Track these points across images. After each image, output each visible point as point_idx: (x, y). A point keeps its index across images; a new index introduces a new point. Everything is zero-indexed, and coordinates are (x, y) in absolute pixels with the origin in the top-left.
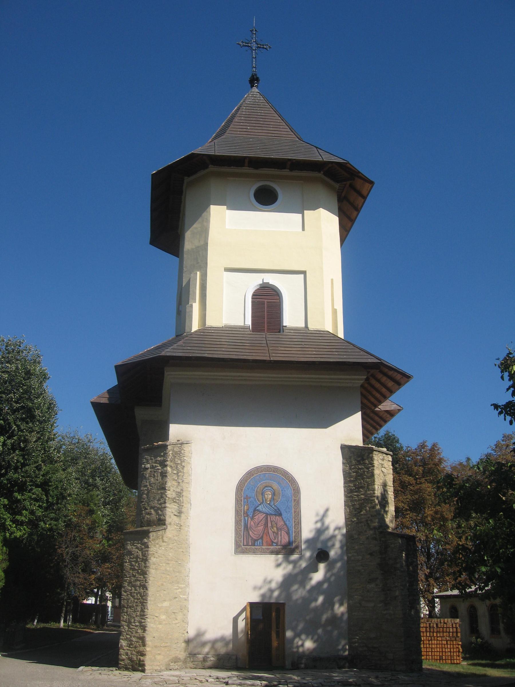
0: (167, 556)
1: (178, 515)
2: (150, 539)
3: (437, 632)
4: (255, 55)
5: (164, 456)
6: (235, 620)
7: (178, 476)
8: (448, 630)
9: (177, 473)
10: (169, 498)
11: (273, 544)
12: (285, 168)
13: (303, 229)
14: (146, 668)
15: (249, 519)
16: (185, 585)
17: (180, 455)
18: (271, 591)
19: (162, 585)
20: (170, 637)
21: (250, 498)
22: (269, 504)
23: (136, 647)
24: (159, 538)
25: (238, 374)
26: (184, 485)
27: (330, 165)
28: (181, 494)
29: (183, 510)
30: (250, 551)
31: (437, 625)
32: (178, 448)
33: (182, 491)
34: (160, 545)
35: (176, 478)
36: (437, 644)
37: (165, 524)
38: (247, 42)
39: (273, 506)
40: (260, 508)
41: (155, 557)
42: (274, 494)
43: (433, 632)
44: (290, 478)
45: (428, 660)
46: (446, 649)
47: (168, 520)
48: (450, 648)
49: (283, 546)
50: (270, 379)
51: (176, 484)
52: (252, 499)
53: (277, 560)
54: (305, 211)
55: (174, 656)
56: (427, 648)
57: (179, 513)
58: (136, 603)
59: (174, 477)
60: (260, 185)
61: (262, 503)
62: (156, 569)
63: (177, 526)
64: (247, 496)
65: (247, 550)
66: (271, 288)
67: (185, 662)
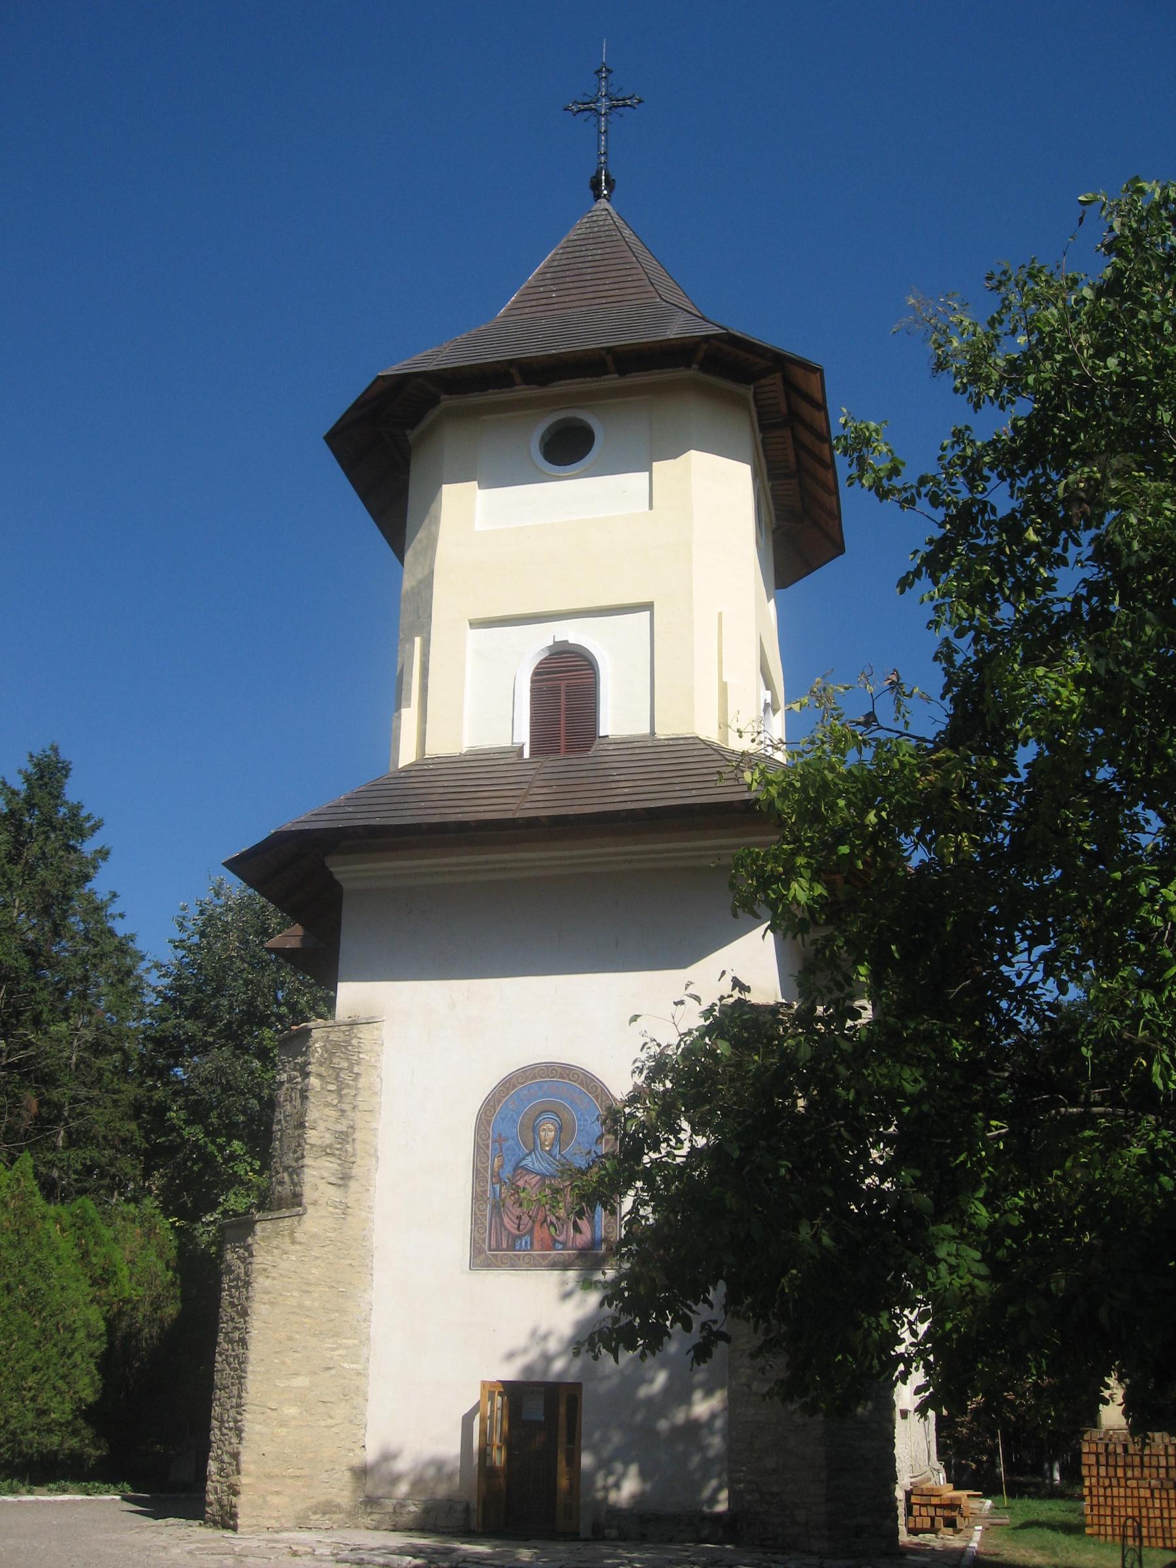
0: (305, 1276)
1: (340, 1182)
2: (256, 1237)
3: (1125, 1466)
4: (606, 126)
5: (304, 1054)
6: (467, 1421)
7: (341, 1097)
8: (1154, 1463)
10: (312, 1146)
11: (557, 1245)
13: (651, 507)
14: (239, 1521)
16: (356, 1342)
17: (348, 1050)
18: (548, 1359)
19: (290, 1339)
20: (311, 1455)
21: (507, 1139)
22: (549, 1152)
23: (227, 1476)
25: (483, 858)
26: (358, 1118)
27: (705, 346)
28: (347, 1136)
29: (354, 1172)
30: (503, 1263)
31: (1125, 1448)
32: (341, 1034)
33: (350, 1130)
35: (335, 1102)
36: (1126, 1497)
37: (300, 1205)
38: (587, 100)
40: (528, 1162)
41: (268, 1277)
42: (560, 1129)
43: (1116, 1466)
44: (599, 1090)
45: (1102, 1538)
46: (1151, 1511)
47: (308, 1194)
48: (1161, 1510)
49: (580, 1249)
50: (603, 859)
51: (334, 1114)
52: (510, 1142)
53: (564, 1283)
54: (654, 464)
55: (322, 1499)
56: (1099, 1505)
58: (233, 1378)
59: (329, 1099)
60: (560, 418)
61: (534, 1150)
62: (272, 1304)
63: (336, 1208)
65: (496, 1258)
66: (576, 653)
67: (352, 1514)
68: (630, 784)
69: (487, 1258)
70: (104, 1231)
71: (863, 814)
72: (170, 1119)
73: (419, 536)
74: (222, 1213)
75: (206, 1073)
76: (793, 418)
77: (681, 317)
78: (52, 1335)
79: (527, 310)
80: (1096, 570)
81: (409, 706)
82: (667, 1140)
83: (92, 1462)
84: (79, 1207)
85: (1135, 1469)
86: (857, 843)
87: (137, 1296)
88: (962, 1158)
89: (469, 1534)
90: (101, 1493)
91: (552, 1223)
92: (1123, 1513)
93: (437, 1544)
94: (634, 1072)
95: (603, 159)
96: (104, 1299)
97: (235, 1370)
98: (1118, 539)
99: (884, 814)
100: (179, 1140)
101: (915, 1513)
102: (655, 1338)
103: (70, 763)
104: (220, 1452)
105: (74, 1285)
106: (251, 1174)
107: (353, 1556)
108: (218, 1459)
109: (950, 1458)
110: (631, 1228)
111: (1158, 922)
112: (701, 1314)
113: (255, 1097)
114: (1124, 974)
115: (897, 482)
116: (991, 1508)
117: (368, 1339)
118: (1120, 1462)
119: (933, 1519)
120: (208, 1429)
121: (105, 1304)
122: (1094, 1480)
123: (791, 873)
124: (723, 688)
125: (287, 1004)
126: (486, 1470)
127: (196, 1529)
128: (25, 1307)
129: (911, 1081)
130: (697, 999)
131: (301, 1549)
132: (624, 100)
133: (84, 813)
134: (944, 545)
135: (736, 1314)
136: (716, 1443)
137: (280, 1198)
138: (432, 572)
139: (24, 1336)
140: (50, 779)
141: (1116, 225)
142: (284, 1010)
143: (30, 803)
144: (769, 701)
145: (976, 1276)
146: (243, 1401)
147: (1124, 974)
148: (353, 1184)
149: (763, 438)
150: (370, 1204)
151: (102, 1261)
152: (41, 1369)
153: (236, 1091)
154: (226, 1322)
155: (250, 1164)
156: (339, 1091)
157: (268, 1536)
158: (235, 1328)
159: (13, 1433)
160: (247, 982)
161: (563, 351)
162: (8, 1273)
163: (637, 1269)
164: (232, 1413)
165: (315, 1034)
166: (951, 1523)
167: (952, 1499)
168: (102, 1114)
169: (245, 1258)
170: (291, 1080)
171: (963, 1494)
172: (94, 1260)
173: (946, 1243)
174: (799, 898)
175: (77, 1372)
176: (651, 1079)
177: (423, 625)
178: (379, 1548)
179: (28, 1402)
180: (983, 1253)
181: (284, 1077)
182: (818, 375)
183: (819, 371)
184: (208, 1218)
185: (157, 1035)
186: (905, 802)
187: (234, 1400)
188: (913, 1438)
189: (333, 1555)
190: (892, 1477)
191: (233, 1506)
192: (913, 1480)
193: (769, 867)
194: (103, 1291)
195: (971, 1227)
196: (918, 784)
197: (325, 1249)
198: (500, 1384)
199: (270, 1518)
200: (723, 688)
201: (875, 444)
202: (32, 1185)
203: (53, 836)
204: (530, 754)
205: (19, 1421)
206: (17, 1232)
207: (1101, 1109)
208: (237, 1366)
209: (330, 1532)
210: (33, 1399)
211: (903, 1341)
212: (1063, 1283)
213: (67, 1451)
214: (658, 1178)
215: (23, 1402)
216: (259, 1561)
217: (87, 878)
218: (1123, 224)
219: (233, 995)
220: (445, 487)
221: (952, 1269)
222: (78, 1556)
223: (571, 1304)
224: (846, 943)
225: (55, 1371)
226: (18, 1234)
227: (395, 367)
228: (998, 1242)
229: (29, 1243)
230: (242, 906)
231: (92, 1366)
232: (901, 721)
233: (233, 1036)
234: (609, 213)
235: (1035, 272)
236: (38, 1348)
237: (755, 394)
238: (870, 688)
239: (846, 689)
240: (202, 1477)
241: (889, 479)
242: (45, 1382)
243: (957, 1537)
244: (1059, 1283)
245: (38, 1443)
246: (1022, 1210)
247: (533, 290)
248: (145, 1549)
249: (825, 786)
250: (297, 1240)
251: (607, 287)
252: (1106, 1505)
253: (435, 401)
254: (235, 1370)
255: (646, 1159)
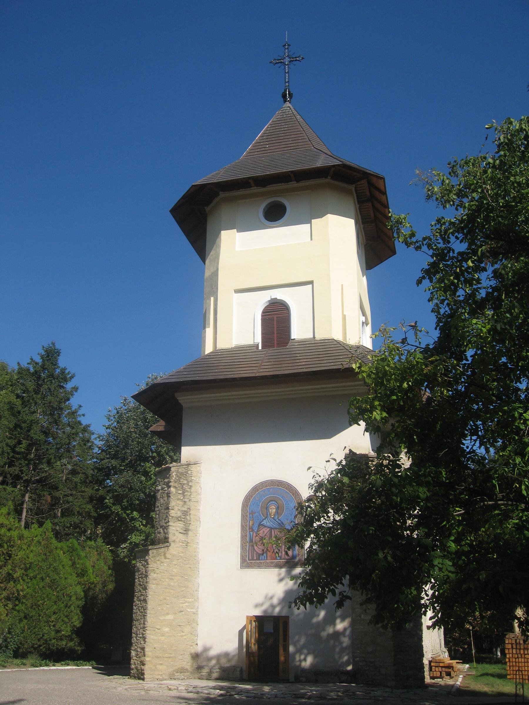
0: (170, 572)
1: (185, 532)
3: (524, 649)
4: (288, 70)
5: (168, 478)
6: (241, 633)
7: (184, 496)
9: (183, 493)
10: (173, 517)
12: (291, 181)
14: (145, 676)
15: (254, 534)
16: (193, 600)
18: (273, 606)
19: (165, 599)
20: (175, 648)
21: (255, 513)
22: (273, 518)
23: (140, 657)
24: (161, 555)
25: (270, 391)
26: (192, 504)
27: (333, 169)
29: (190, 528)
30: (254, 565)
32: (184, 469)
34: (161, 562)
35: (182, 498)
37: (168, 542)
38: (279, 58)
39: (277, 520)
40: (264, 522)
41: (155, 573)
42: (278, 508)
43: (520, 649)
44: (294, 491)
47: (171, 538)
51: (181, 503)
52: (257, 514)
53: (280, 574)
54: (312, 220)
55: (180, 666)
56: (513, 666)
57: (185, 531)
59: (179, 497)
60: (269, 202)
63: (183, 543)
64: (252, 511)
68: (305, 360)
69: (248, 563)
70: (81, 553)
71: (402, 383)
72: (106, 503)
73: (212, 253)
74: (129, 543)
75: (121, 482)
76: (372, 198)
77: (323, 156)
78: (61, 599)
79: (256, 153)
80: (495, 282)
81: (209, 327)
82: (324, 516)
83: (80, 652)
84: (71, 543)
85: (510, 650)
86: (399, 395)
87: (96, 581)
88: (444, 523)
89: (242, 681)
90: (83, 666)
91: (276, 552)
92: (523, 669)
93: (230, 685)
94: (309, 488)
95: (287, 84)
96: (83, 582)
97: (142, 612)
98: (503, 272)
99: (410, 383)
100: (110, 512)
101: (433, 670)
102: (321, 599)
103: (60, 350)
104: (136, 647)
105: (70, 577)
106: (142, 526)
107: (194, 690)
108: (135, 650)
109: (451, 646)
110: (310, 554)
111: (522, 427)
112: (339, 588)
113: (143, 492)
114: (509, 449)
115: (414, 239)
116: (468, 668)
117: (198, 598)
118: (522, 647)
119: (441, 672)
120: (131, 638)
121: (83, 584)
122: (511, 655)
123: (373, 408)
124: (344, 317)
125: (156, 452)
126: (249, 653)
127: (127, 680)
128: (50, 587)
129: (423, 492)
130: (335, 460)
131: (173, 687)
132: (296, 58)
133: (67, 372)
134: (434, 266)
135: (354, 589)
136: (346, 641)
137: (159, 539)
138: (218, 269)
139: (49, 599)
140: (52, 357)
141: (502, 138)
142: (155, 454)
143: (43, 368)
144: (364, 321)
145: (450, 572)
146: (146, 626)
147: (509, 449)
148: (190, 533)
149: (360, 206)
150: (198, 541)
151: (81, 566)
152: (57, 613)
153: (135, 490)
154: (138, 592)
155: (141, 522)
156: (183, 493)
157: (158, 682)
158: (142, 595)
159: (46, 640)
160: (138, 443)
161: (272, 173)
162: (42, 572)
163: (313, 572)
164: (141, 631)
165: (172, 469)
166: (449, 674)
167: (449, 664)
168: (77, 502)
169: (145, 565)
170: (162, 489)
171: (454, 662)
172: (78, 566)
173: (437, 558)
174: (377, 418)
175: (73, 614)
176: (316, 491)
177: (214, 292)
178: (205, 687)
179: (52, 627)
180: (453, 563)
181: (160, 488)
182: (383, 180)
183: (383, 179)
184: (123, 546)
185: (100, 467)
186: (419, 378)
187: (142, 625)
188: (433, 638)
189: (186, 690)
190: (421, 655)
191: (142, 670)
192: (433, 656)
193: (364, 406)
194: (82, 579)
195: (448, 552)
196: (424, 371)
197: (179, 561)
198: (254, 617)
199: (158, 675)
200: (344, 317)
201: (404, 224)
202: (51, 534)
203: (53, 381)
204: (262, 347)
205: (48, 635)
206: (45, 554)
207: (502, 502)
208: (143, 611)
209: (184, 680)
210: (54, 626)
211: (423, 598)
212: (485, 576)
213: (68, 648)
214: (320, 533)
215: (50, 627)
216: (155, 692)
217: (68, 399)
218: (504, 137)
219: (132, 448)
220: (222, 232)
221: (440, 569)
222: (80, 691)
223: (284, 582)
224: (395, 436)
225: (63, 613)
226: (46, 555)
227: (200, 181)
228: (459, 558)
229: (50, 559)
230: (135, 409)
231: (78, 611)
232: (418, 342)
233: (132, 466)
234: (290, 108)
235: (467, 161)
236: (55, 604)
237: (355, 188)
238: (404, 329)
239: (394, 329)
240: (128, 658)
241: (411, 238)
242: (59, 618)
243: (451, 680)
244: (483, 576)
245: (57, 645)
246: (468, 544)
247: (258, 144)
248: (107, 688)
249: (385, 373)
250: (167, 557)
251: (290, 142)
252: (516, 666)
253: (217, 195)
254: (142, 612)
255: (315, 525)
